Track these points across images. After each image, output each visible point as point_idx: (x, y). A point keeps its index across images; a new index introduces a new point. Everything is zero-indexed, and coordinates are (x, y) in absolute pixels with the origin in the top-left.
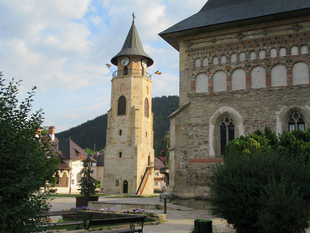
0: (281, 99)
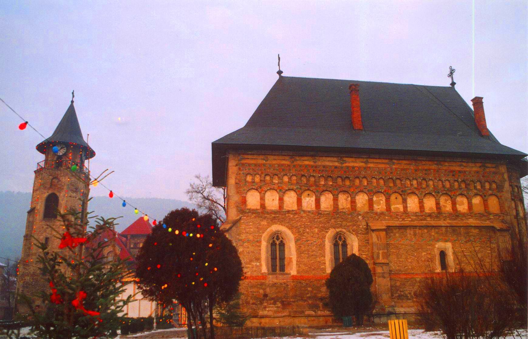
0: (329, 222)
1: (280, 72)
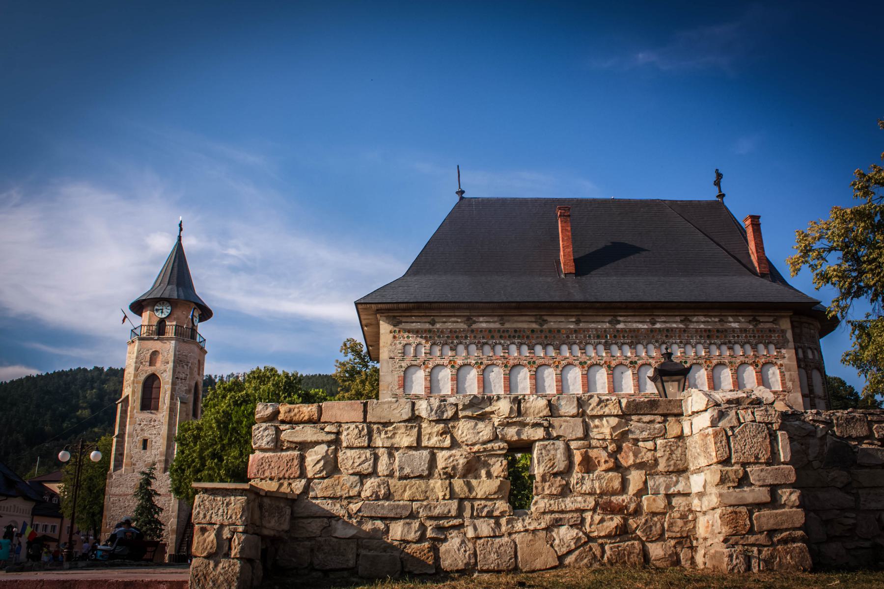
1: (461, 192)
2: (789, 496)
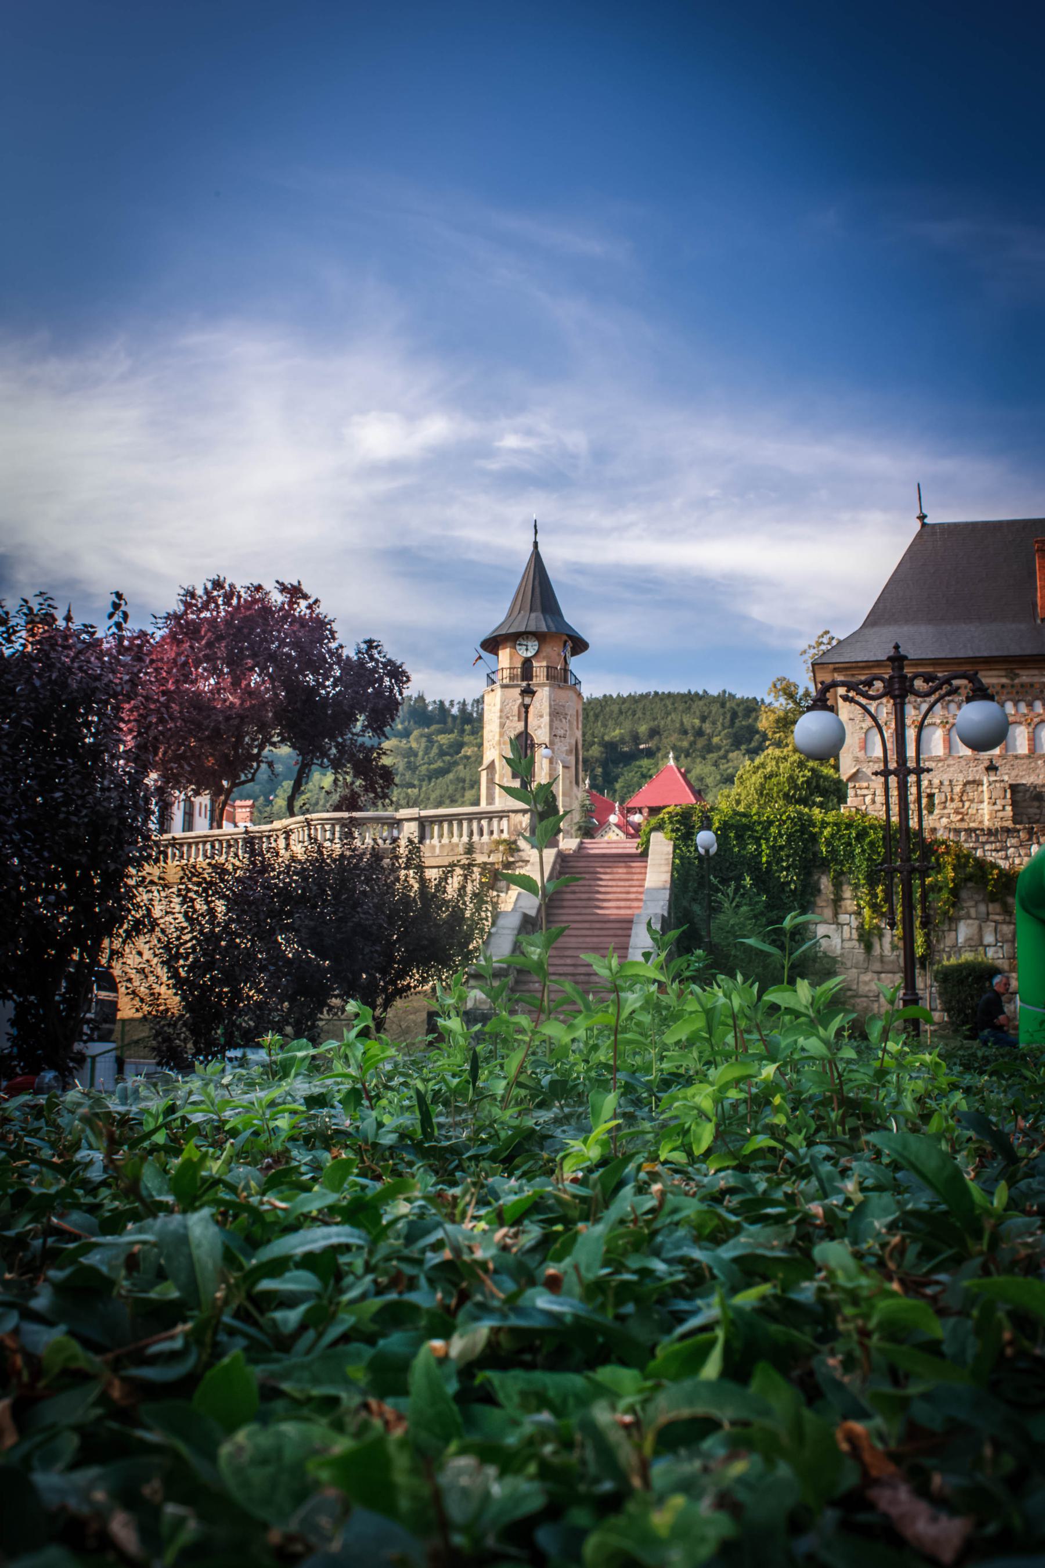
2: (1009, 808)
